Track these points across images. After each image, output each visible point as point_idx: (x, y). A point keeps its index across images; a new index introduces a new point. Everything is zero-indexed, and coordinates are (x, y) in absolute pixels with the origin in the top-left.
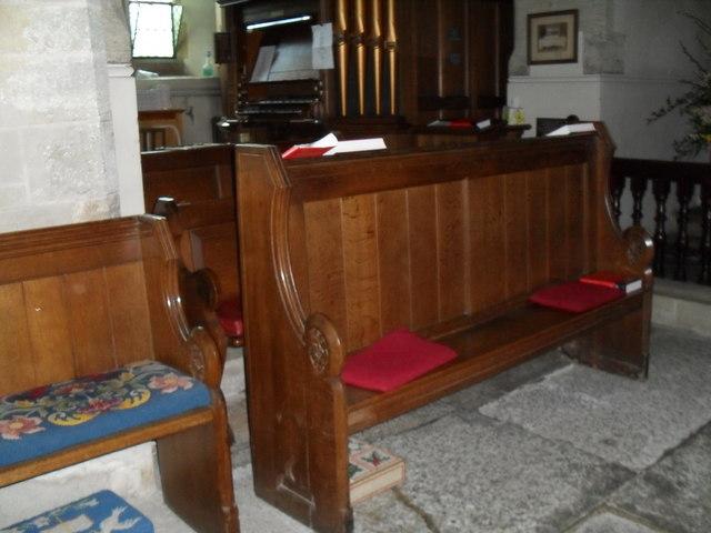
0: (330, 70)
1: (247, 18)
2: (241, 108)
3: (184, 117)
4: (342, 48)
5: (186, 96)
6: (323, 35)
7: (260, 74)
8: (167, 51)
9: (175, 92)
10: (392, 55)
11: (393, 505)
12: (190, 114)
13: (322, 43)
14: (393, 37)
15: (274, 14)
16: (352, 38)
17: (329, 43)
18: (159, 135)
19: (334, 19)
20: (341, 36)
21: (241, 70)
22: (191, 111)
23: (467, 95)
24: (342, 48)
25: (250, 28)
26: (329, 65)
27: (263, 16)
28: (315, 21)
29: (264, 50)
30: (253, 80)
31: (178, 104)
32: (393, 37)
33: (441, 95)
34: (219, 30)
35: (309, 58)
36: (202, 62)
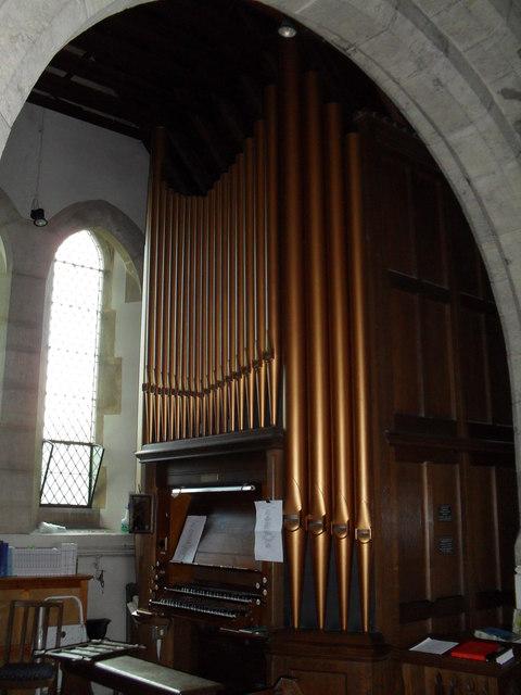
0: (278, 564)
1: (172, 480)
2: (159, 595)
3: (93, 584)
4: (296, 535)
5: (98, 556)
6: (269, 515)
7: (184, 553)
8: (80, 497)
9: (85, 550)
10: (365, 548)
11: (394, 19)
12: (100, 578)
13: (266, 526)
14: (366, 522)
15: (205, 478)
16: (309, 522)
17: (277, 527)
18: (54, 614)
19: (285, 494)
20: (296, 517)
21: (162, 544)
22: (102, 575)
23: (455, 419)
24: (296, 535)
25: (176, 491)
26: (276, 556)
27: (194, 479)
28: (261, 494)
29: (191, 519)
30: (176, 559)
31: (86, 569)
32: (366, 522)
33: (429, 597)
34: (137, 492)
35: (250, 539)
36: (117, 514)
